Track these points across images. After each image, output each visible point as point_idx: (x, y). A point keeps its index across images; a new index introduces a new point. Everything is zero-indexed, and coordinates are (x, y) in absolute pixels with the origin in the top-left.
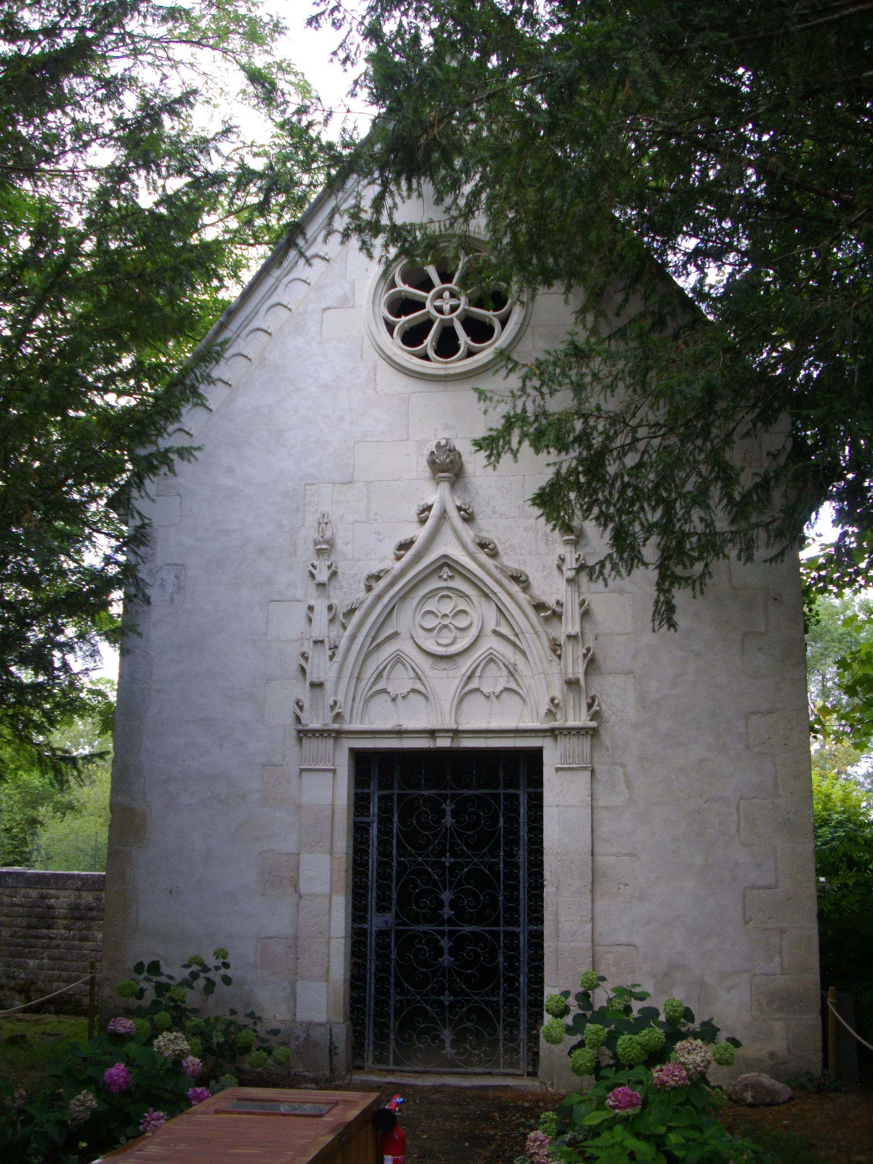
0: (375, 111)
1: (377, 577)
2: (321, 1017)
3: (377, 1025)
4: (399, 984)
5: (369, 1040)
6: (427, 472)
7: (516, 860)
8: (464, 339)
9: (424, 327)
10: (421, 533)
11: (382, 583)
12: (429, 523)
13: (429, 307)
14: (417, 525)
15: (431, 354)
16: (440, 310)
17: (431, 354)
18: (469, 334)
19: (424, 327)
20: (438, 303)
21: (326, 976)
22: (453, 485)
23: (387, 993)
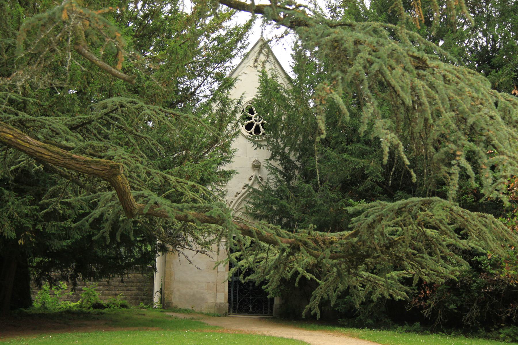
0: (193, 5)
1: (239, 194)
2: (223, 301)
3: (234, 304)
4: (239, 294)
5: (232, 309)
6: (251, 166)
7: (231, 313)
8: (253, 130)
9: (251, 124)
10: (250, 183)
11: (239, 195)
12: (252, 180)
13: (253, 120)
14: (248, 180)
15: (253, 133)
16: (256, 121)
17: (253, 133)
18: (255, 129)
19: (251, 124)
20: (256, 119)
21: (224, 292)
22: (258, 170)
23: (236, 296)
